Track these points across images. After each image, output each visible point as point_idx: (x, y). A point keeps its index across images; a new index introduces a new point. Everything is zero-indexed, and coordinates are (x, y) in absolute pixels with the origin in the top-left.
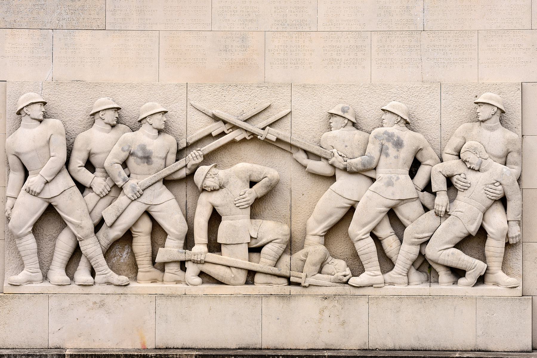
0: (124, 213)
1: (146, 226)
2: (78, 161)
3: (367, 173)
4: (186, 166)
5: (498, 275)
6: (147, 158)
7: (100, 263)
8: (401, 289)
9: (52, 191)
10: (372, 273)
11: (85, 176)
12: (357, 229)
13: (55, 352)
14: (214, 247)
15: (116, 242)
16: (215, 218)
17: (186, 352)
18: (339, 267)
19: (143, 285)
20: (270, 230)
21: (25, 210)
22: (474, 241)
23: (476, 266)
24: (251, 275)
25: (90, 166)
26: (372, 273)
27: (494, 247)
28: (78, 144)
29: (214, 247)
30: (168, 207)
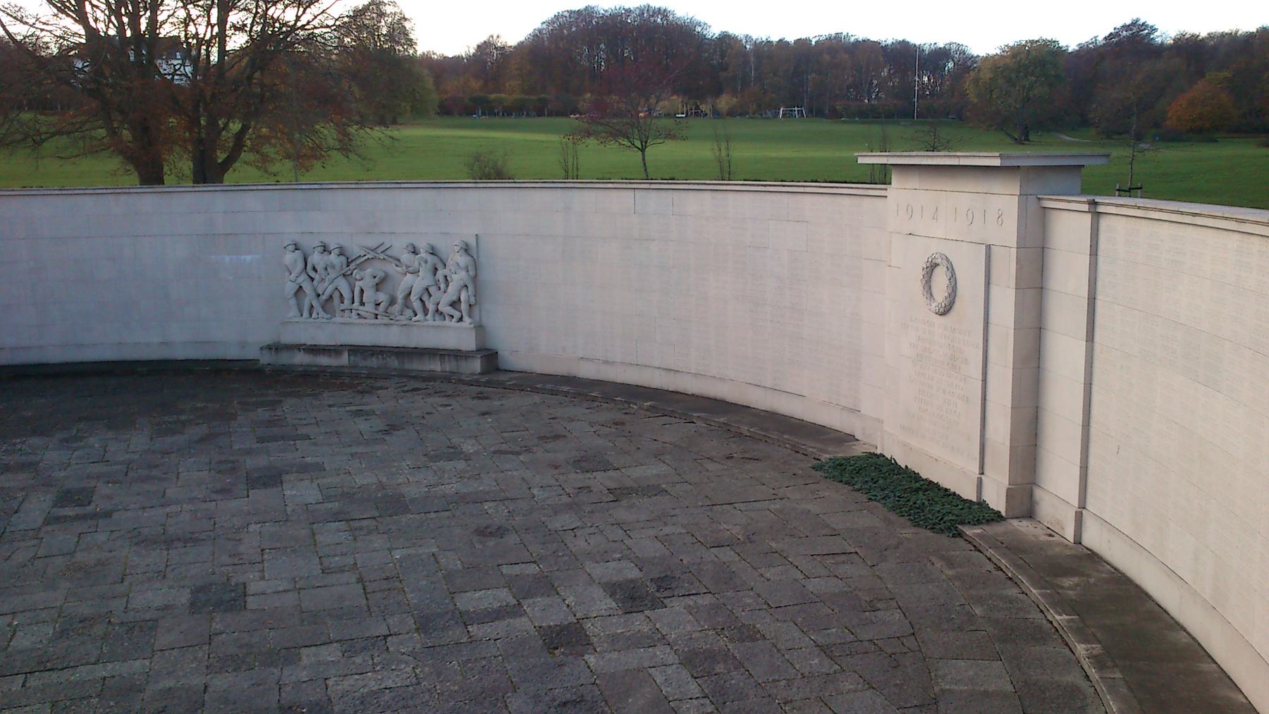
0: (327, 289)
1: (336, 295)
2: (309, 267)
3: (416, 272)
4: (72, 554)
5: (466, 318)
6: (333, 267)
7: (320, 310)
8: (431, 322)
9: (300, 280)
10: (420, 316)
11: (312, 274)
12: (413, 298)
13: (660, 151)
14: (362, 304)
15: (327, 301)
16: (362, 291)
17: (324, 360)
18: (409, 313)
19: (338, 319)
20: (382, 297)
21: (290, 288)
22: (455, 304)
23: (457, 314)
24: (376, 316)
25: (315, 269)
26: (420, 316)
27: (464, 306)
28: (309, 260)
29: (362, 304)
30: (343, 286)
